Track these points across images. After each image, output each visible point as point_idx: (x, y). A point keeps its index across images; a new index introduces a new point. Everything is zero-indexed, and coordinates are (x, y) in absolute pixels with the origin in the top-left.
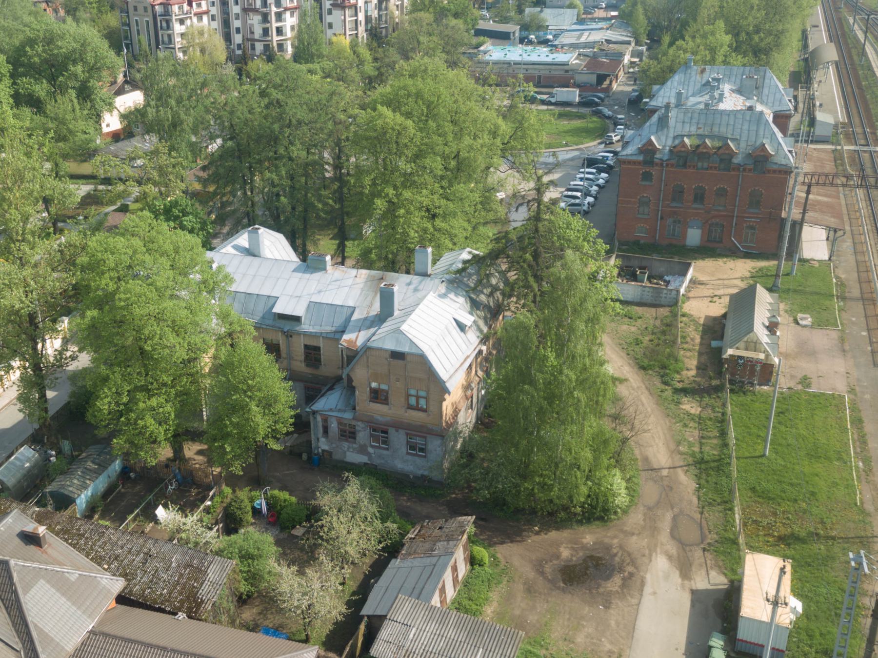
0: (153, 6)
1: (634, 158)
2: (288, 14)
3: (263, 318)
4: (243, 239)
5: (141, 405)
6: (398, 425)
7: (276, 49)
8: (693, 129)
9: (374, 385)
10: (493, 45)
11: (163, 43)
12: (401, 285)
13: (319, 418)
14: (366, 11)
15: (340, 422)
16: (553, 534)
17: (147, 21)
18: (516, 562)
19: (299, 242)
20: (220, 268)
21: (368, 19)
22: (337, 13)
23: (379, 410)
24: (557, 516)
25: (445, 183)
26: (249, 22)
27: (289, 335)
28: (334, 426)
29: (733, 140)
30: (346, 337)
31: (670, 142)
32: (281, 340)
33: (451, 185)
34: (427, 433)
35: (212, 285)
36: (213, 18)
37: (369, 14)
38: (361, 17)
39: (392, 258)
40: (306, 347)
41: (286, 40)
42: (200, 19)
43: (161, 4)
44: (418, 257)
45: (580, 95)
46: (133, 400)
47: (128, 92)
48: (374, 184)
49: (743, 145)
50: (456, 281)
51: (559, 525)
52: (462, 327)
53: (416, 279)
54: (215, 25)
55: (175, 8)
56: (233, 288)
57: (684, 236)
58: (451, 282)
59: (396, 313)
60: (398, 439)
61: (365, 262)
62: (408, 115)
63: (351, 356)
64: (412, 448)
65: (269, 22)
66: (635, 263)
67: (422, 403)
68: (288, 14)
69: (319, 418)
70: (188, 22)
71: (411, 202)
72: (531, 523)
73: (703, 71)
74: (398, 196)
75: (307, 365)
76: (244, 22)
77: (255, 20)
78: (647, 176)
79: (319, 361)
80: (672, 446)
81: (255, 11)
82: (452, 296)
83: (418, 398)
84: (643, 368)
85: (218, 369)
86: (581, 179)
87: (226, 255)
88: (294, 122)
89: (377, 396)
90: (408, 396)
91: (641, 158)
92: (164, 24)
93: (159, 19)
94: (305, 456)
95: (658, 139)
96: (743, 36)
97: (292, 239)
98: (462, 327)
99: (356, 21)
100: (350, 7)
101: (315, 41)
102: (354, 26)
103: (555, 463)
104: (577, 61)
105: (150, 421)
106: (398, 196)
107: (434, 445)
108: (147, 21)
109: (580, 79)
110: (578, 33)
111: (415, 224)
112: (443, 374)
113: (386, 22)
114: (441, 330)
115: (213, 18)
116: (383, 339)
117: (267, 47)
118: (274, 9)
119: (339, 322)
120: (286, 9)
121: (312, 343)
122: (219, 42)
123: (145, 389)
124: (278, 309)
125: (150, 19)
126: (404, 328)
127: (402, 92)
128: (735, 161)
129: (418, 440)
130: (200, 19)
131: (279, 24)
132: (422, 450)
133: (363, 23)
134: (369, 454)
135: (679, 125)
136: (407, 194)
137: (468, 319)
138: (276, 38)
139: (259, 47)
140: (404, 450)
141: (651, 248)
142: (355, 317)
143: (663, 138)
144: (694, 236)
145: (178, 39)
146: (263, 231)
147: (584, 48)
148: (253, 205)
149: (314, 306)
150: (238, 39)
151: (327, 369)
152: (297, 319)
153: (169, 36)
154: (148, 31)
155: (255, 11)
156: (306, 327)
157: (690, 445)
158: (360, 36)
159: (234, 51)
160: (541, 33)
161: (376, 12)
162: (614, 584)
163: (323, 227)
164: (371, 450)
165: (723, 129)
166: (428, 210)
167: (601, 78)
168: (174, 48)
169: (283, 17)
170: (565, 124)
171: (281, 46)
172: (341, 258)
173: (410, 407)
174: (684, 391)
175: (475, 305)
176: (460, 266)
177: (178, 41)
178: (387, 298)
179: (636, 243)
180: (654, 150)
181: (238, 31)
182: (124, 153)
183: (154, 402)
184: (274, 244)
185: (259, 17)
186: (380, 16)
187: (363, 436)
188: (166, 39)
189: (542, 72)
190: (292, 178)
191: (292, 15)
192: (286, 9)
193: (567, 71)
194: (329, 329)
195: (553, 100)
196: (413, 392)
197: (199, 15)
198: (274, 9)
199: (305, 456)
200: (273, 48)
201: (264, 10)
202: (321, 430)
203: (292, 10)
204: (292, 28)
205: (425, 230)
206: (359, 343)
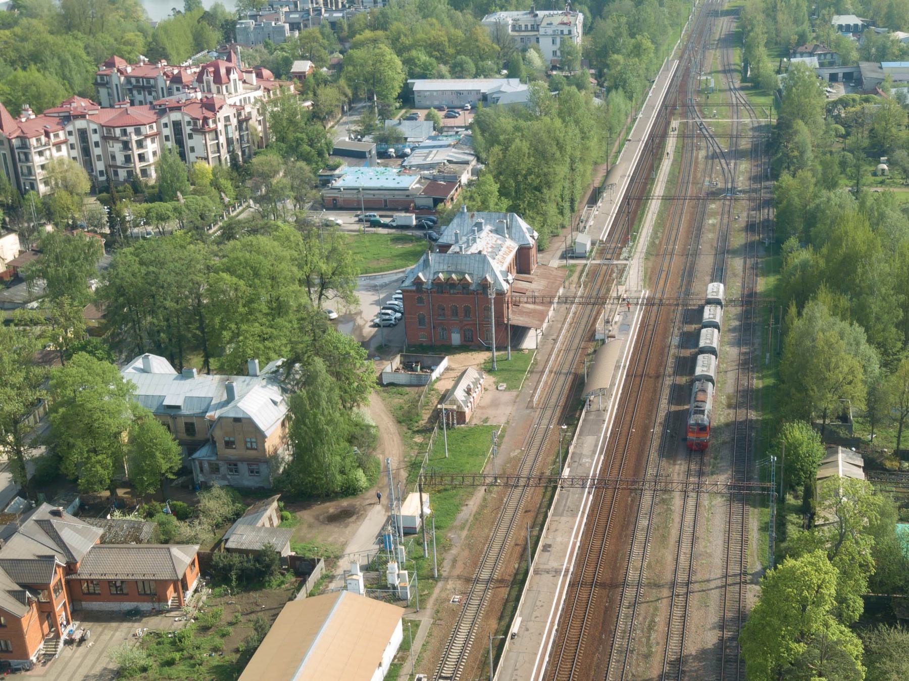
0: (9, 140)
1: (410, 288)
2: (149, 141)
3: (158, 409)
4: (139, 363)
5: (93, 460)
6: (242, 460)
7: (140, 175)
8: (445, 267)
9: (227, 439)
10: (350, 165)
11: (22, 174)
12: (238, 383)
13: (197, 463)
14: (227, 133)
15: (210, 464)
16: (328, 504)
17: (4, 154)
18: (305, 517)
19: (176, 361)
20: (128, 382)
21: (229, 142)
22: (197, 138)
23: (231, 453)
24: (329, 496)
25: (270, 318)
26: (110, 149)
27: (174, 417)
28: (206, 465)
29: (469, 274)
30: (208, 414)
31: (431, 277)
32: (170, 421)
33: (273, 320)
34: (261, 461)
35: (124, 391)
36: (72, 147)
37: (230, 136)
38: (222, 139)
39: (239, 367)
40: (186, 424)
41: (150, 165)
42: (59, 149)
43: (17, 137)
44: (250, 366)
45: (416, 218)
46: (88, 458)
47: (4, 236)
48: (222, 322)
49: (475, 277)
50: (273, 378)
51: (331, 500)
52: (275, 403)
53: (248, 378)
54: (74, 153)
55: (33, 141)
56: (137, 392)
57: (450, 338)
58: (270, 378)
59: (236, 398)
60: (243, 468)
61: (221, 370)
62: (240, 277)
63: (212, 423)
64: (252, 472)
65: (130, 150)
66: (413, 359)
67: (254, 445)
68: (149, 141)
69: (197, 463)
70: (47, 153)
71: (247, 331)
72: (316, 501)
73: (472, 216)
74: (238, 328)
75: (188, 435)
76: (105, 150)
77: (116, 148)
78: (420, 300)
79: (194, 431)
80: (402, 459)
81: (116, 139)
82: (270, 386)
83: (251, 442)
84: (400, 422)
85: (132, 440)
86: (396, 299)
87: (130, 373)
88: (166, 285)
89: (229, 444)
90: (246, 442)
91: (414, 288)
92: (22, 157)
93: (16, 151)
94: (191, 487)
95: (424, 275)
96: (520, 178)
97: (171, 360)
98: (275, 403)
99: (218, 144)
100: (211, 131)
101: (178, 179)
102: (216, 149)
103: (321, 465)
104: (418, 185)
105: (99, 467)
106: (238, 328)
107: (263, 468)
108: (4, 154)
109: (421, 202)
110: (427, 151)
111: (252, 344)
112: (262, 426)
113: (248, 142)
114: (262, 405)
115: (72, 147)
116: (228, 412)
117: (130, 173)
118: (134, 138)
119: (204, 407)
120: (146, 137)
121: (189, 421)
122: (79, 168)
123: (95, 451)
124: (166, 403)
125: (7, 152)
126: (239, 405)
127: (236, 262)
128: (472, 288)
129: (254, 467)
130: (59, 149)
131: (141, 151)
132: (257, 472)
133: (225, 145)
134: (228, 479)
135: (437, 265)
136: (244, 327)
137: (278, 398)
138: (139, 165)
139: (122, 174)
140: (247, 474)
141: (424, 349)
142: (213, 403)
143: (427, 274)
144: (456, 338)
145: (38, 171)
146: (152, 357)
147: (428, 169)
148: (141, 338)
149: (188, 399)
150: (100, 166)
151: (199, 436)
152: (178, 407)
153: (29, 168)
154: (6, 163)
155: (116, 139)
156: (185, 411)
157: (411, 457)
158: (223, 158)
159: (96, 177)
160: (400, 146)
161: (237, 133)
162: (354, 517)
163: (194, 349)
164: (229, 477)
165: (463, 267)
166: (259, 336)
167: (437, 201)
168: (35, 180)
169: (144, 144)
170: (400, 248)
171: (144, 172)
172: (206, 369)
173: (248, 449)
174: (418, 432)
175: (284, 390)
176: (275, 369)
177: (40, 174)
178: (230, 390)
179: (421, 346)
180: (422, 283)
181: (99, 158)
182: (19, 298)
183: (100, 457)
184: (160, 364)
185: (120, 145)
186: (241, 137)
187: (223, 469)
188: (25, 171)
189: (387, 197)
190: (167, 320)
191: (153, 142)
192: (146, 137)
193: (408, 196)
194: (198, 411)
195: (394, 224)
196: (248, 440)
197: (58, 146)
198: (134, 138)
199: (191, 487)
200: (137, 175)
201: (125, 138)
202: (199, 469)
203: (153, 137)
204: (154, 153)
205: (258, 349)
206: (216, 417)
